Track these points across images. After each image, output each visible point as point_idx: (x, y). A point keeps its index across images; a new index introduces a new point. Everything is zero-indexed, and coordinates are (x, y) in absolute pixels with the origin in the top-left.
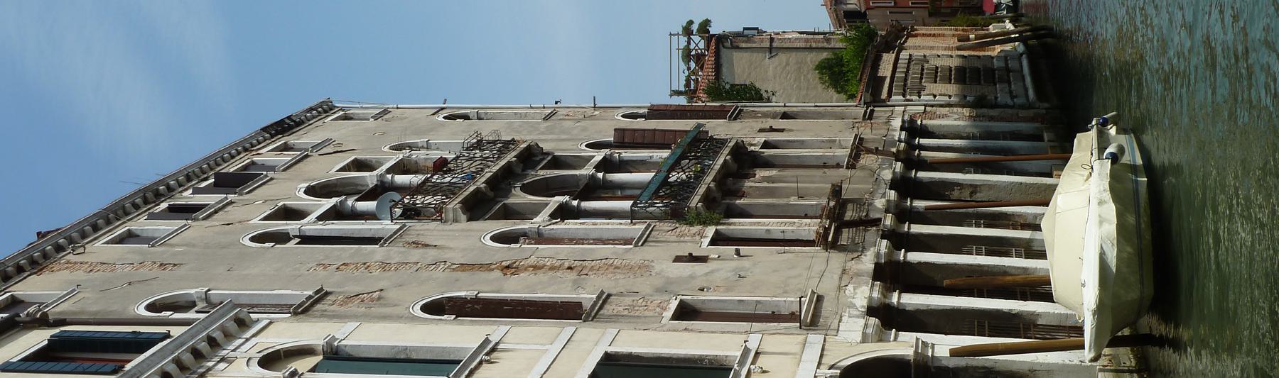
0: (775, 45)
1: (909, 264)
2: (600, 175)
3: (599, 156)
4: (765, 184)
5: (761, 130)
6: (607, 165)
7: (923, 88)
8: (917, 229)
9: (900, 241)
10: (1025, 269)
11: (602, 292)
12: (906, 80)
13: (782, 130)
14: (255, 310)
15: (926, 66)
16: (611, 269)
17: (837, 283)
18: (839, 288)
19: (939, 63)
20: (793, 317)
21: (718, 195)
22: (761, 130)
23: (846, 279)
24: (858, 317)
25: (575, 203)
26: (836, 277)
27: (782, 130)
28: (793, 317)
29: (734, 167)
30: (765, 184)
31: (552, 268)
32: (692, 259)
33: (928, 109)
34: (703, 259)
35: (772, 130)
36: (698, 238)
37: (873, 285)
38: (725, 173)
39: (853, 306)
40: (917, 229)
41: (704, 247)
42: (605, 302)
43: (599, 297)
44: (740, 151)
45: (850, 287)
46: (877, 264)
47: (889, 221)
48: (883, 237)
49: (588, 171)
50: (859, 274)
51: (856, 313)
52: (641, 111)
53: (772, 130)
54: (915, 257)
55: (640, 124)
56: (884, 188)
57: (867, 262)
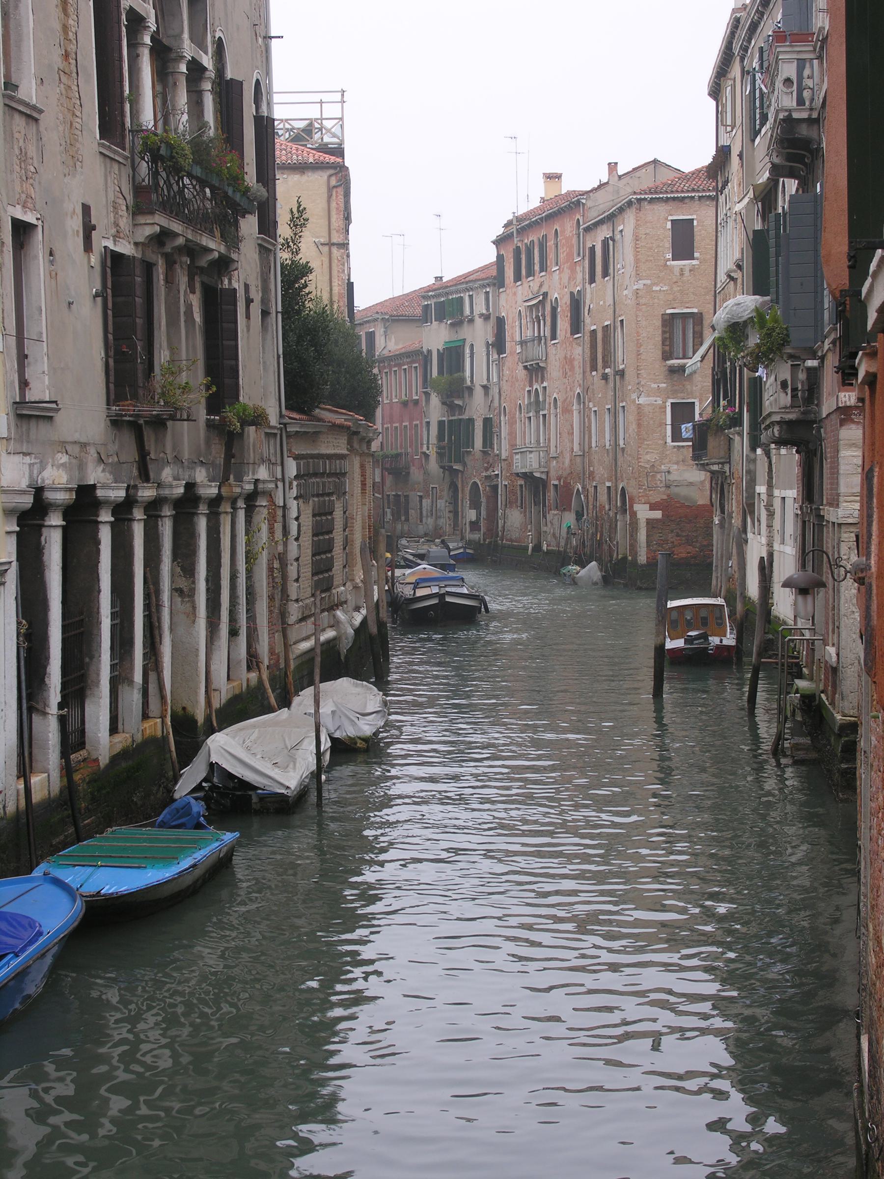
0: (334, 250)
1: (97, 531)
2: (183, 68)
3: (207, 61)
4: (182, 309)
5: (247, 286)
6: (196, 69)
7: (306, 501)
8: (138, 531)
9: (122, 511)
10: (97, 683)
11: (41, 111)
12: (315, 475)
13: (248, 317)
14: (505, 776)
15: (334, 498)
16: (69, 116)
17: (69, 439)
18: (63, 444)
19: (338, 514)
20: (24, 384)
21: (168, 249)
22: (247, 286)
23: (75, 450)
24: (31, 476)
25: (147, 40)
26: (76, 437)
27: (248, 317)
28: (24, 384)
29: (203, 262)
30: (182, 309)
31: (65, 28)
32: (88, 229)
33: (280, 513)
34: (88, 246)
35: (249, 301)
36: (113, 231)
37: (70, 490)
38: (193, 250)
39: (43, 469)
40: (138, 531)
41: (103, 241)
42: (29, 116)
43: (34, 108)
44: (224, 265)
45: (63, 459)
46: (94, 487)
47: (147, 493)
48: (128, 489)
49: (188, 49)
50: (82, 467)
51: (35, 475)
52: (264, 107)
53: (249, 301)
54: (105, 535)
55: (249, 110)
56: (186, 478)
57: (95, 475)
